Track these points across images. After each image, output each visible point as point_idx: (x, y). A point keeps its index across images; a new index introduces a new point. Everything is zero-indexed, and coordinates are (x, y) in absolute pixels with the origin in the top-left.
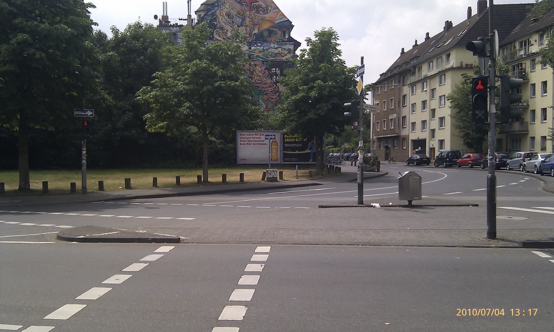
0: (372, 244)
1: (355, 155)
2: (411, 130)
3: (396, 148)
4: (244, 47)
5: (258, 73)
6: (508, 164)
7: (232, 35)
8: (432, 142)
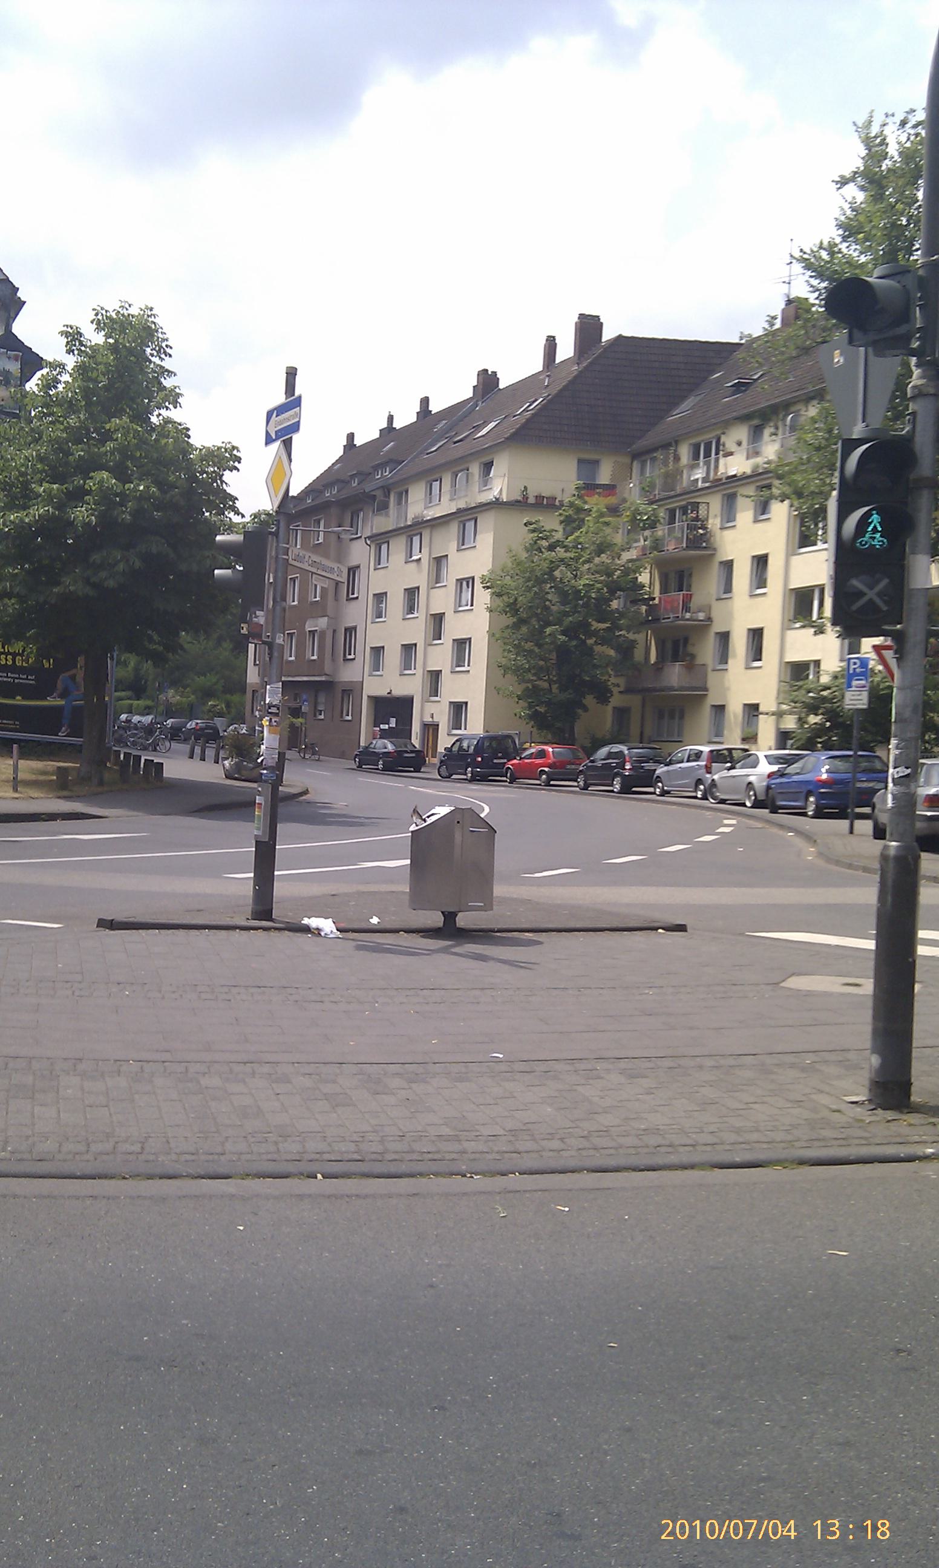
0: (378, 1168)
2: (370, 667)
3: (322, 717)
6: (658, 777)
8: (430, 708)
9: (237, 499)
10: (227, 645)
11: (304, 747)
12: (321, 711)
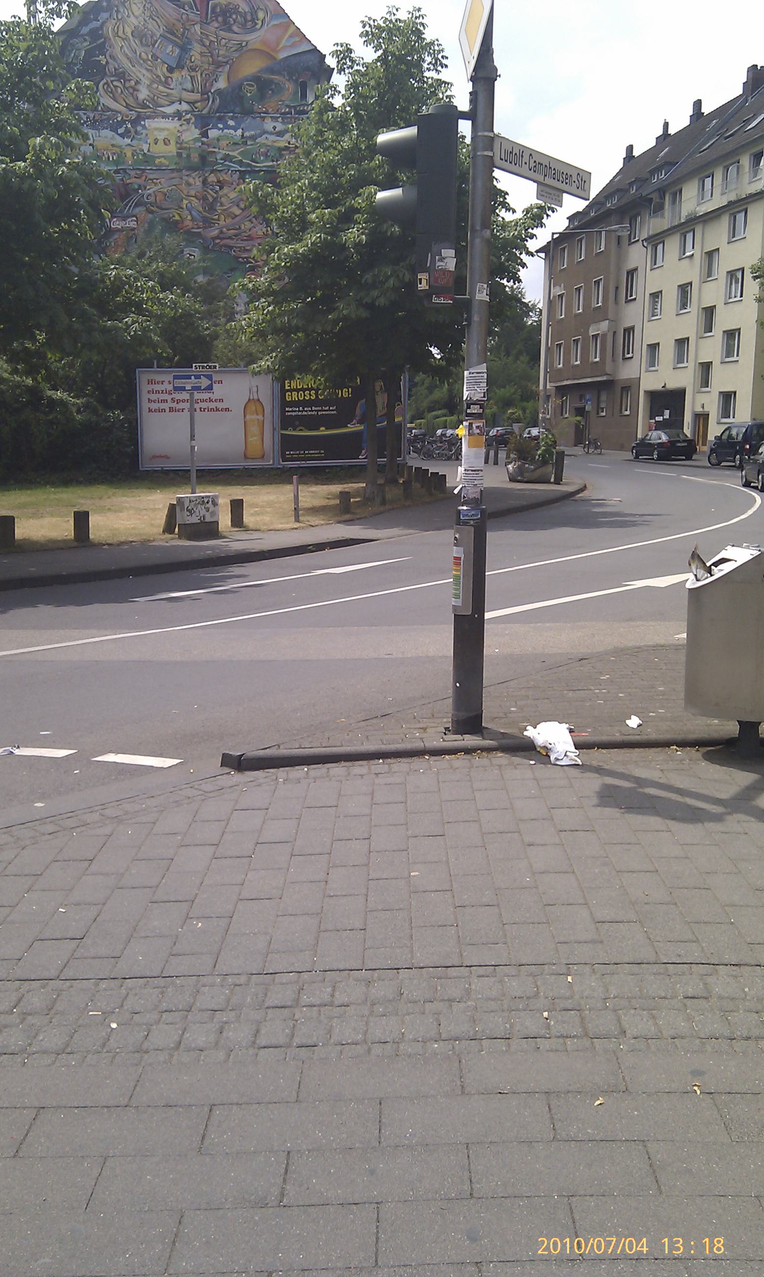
1: (499, 434)
2: (646, 364)
3: (604, 414)
4: (187, 130)
5: (230, 208)
7: (152, 96)
9: (507, 194)
10: (524, 358)
11: (587, 443)
12: (603, 408)
